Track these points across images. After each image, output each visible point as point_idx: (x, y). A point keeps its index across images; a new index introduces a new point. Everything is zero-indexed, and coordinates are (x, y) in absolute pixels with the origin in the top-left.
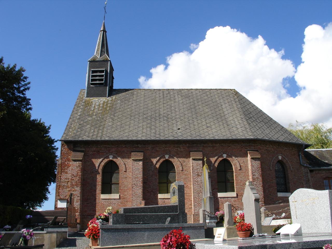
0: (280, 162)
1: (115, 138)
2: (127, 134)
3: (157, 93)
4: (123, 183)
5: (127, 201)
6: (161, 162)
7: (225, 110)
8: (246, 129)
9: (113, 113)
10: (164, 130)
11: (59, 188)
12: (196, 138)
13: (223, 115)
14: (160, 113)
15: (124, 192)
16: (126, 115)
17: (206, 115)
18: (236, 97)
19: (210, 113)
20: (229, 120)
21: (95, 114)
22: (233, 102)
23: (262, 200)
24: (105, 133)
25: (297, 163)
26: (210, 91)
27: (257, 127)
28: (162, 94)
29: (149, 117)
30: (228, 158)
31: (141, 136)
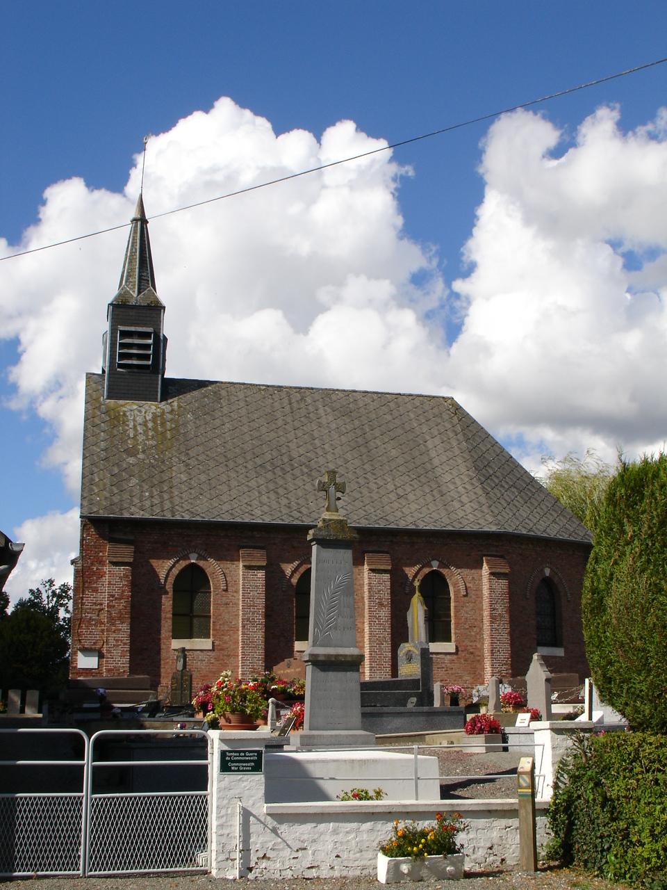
0: (547, 582)
1: (203, 515)
2: (226, 507)
3: (276, 397)
4: (220, 615)
5: (229, 656)
6: (302, 572)
7: (433, 454)
8: (481, 505)
9: (183, 448)
10: (307, 500)
11: (80, 624)
12: (378, 524)
13: (428, 466)
14: (290, 456)
15: (223, 635)
16: (215, 455)
17: (393, 465)
18: (455, 420)
19: (400, 461)
20: (444, 481)
21: (140, 447)
22: (451, 434)
23: (507, 661)
24: (177, 500)
26: (396, 399)
27: (503, 502)
28: (287, 401)
29: (268, 463)
30: (441, 570)
31: (260, 513)
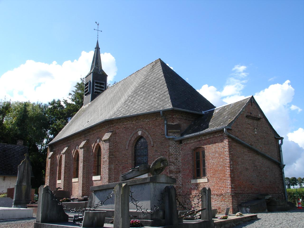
25: (162, 135)
